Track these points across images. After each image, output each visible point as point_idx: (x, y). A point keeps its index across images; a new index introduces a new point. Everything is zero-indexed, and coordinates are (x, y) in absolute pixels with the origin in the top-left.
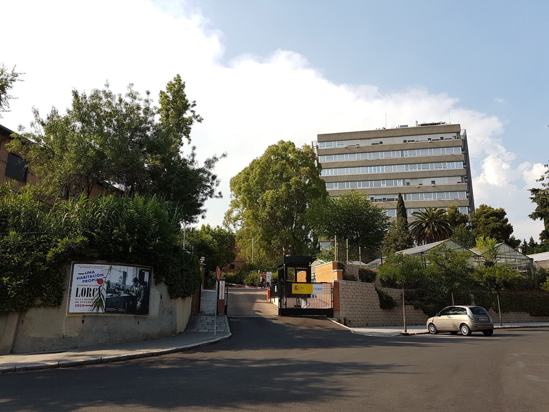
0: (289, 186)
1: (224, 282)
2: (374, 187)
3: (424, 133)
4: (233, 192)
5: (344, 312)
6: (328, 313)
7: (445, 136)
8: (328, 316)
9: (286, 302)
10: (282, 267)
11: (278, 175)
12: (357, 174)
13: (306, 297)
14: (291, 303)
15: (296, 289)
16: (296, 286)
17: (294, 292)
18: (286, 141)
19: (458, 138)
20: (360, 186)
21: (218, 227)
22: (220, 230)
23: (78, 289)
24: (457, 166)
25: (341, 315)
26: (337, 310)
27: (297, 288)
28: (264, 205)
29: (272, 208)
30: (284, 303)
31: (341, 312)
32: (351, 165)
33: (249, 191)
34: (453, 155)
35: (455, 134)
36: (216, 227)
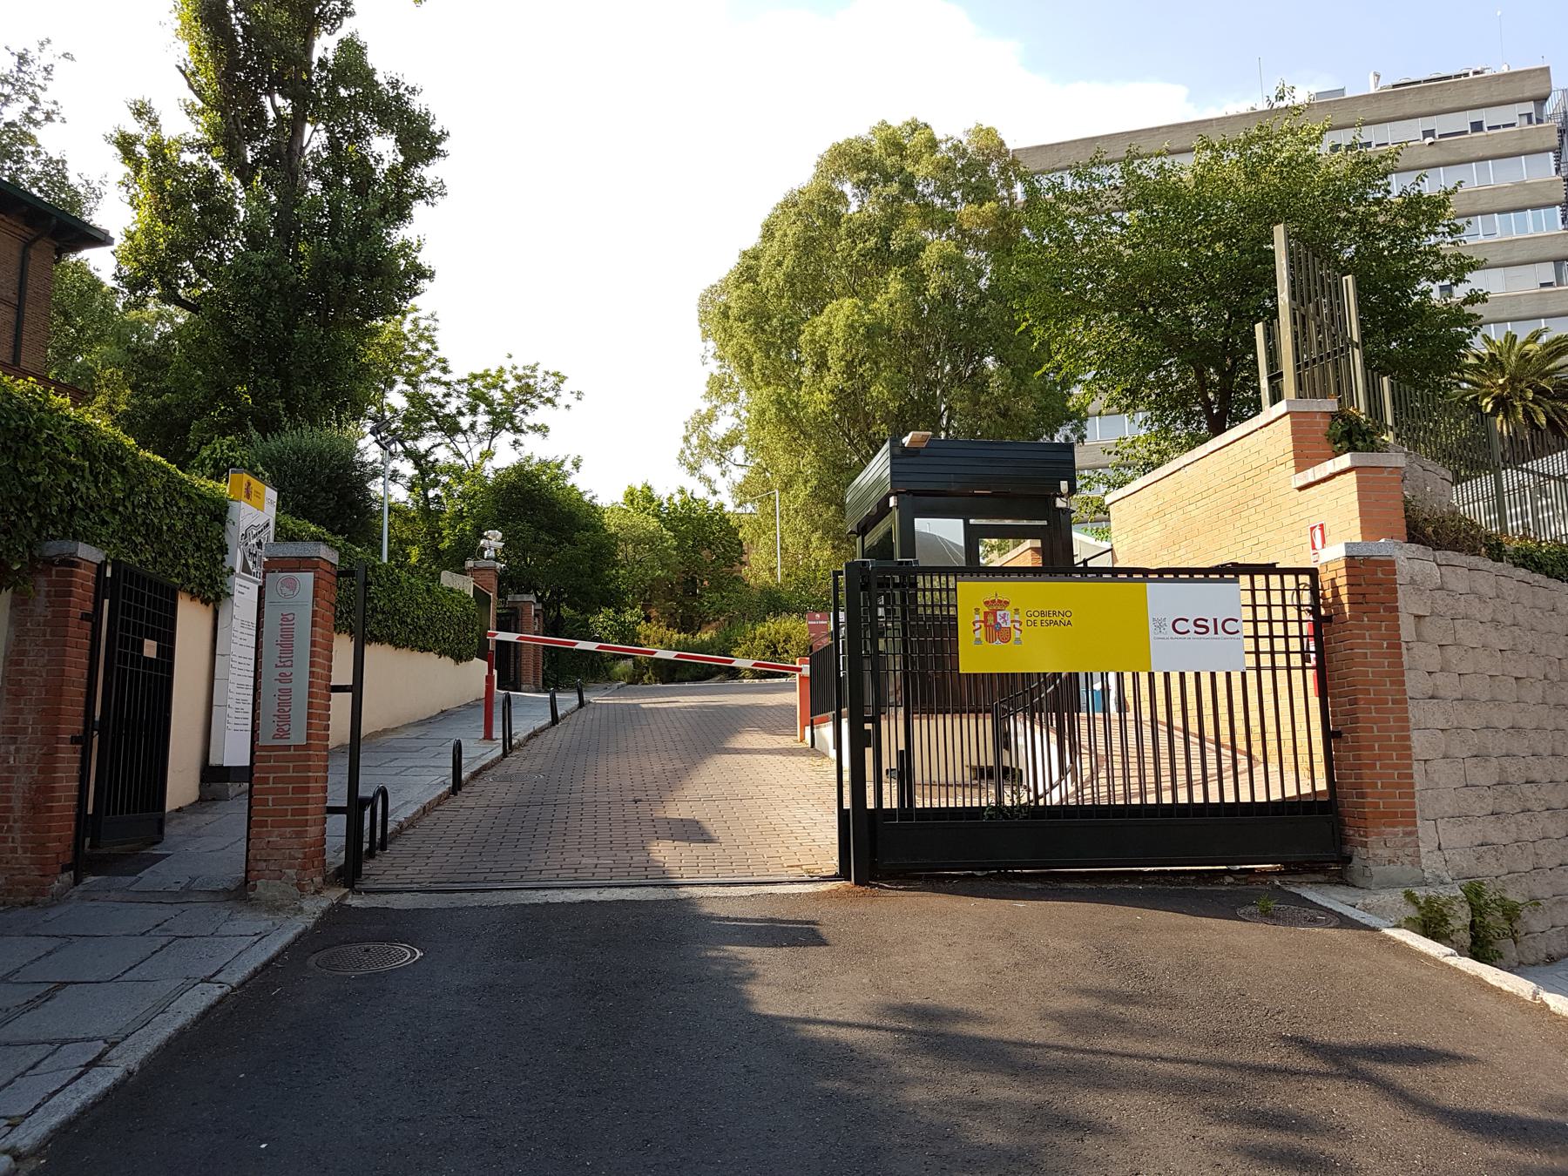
0: (916, 281)
3: (1409, 110)
4: (711, 344)
5: (1453, 835)
6: (1293, 850)
7: (1488, 117)
8: (1295, 869)
9: (906, 757)
10: (881, 528)
11: (873, 240)
13: (1057, 699)
14: (944, 759)
15: (996, 632)
16: (996, 605)
17: (976, 656)
18: (896, 122)
19: (1539, 121)
21: (682, 491)
22: (689, 502)
24: (1538, 226)
25: (1431, 863)
26: (1391, 818)
27: (1006, 618)
28: (821, 366)
29: (850, 370)
30: (889, 761)
31: (1424, 829)
33: (758, 316)
34: (1523, 185)
35: (1530, 107)
36: (674, 491)
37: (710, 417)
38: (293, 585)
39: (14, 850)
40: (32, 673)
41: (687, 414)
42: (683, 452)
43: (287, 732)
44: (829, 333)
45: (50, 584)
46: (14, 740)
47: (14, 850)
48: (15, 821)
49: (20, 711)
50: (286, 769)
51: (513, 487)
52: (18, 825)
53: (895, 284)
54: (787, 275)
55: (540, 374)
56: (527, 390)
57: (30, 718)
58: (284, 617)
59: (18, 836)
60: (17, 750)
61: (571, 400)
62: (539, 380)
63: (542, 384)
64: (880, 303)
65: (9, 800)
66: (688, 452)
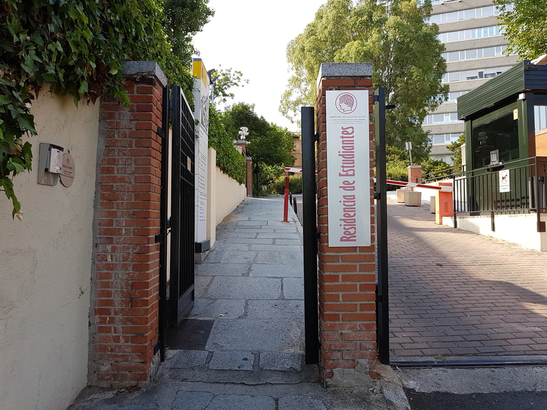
1: (362, 97)
2: (483, 58)
12: (459, 40)
20: (462, 57)
23: (493, 229)
32: (451, 29)
37: (289, 94)
38: (350, 102)
39: (117, 339)
40: (122, 180)
41: (283, 92)
42: (280, 107)
43: (353, 235)
44: (348, 55)
45: (133, 99)
46: (110, 241)
47: (117, 339)
48: (116, 313)
49: (114, 214)
50: (354, 268)
51: (240, 112)
52: (120, 316)
53: (375, 35)
54: (329, 32)
55: (232, 73)
56: (227, 79)
57: (123, 221)
58: (345, 131)
59: (119, 326)
60: (114, 249)
61: (244, 83)
62: (232, 75)
63: (232, 77)
64: (369, 43)
65: (109, 294)
66: (282, 107)
